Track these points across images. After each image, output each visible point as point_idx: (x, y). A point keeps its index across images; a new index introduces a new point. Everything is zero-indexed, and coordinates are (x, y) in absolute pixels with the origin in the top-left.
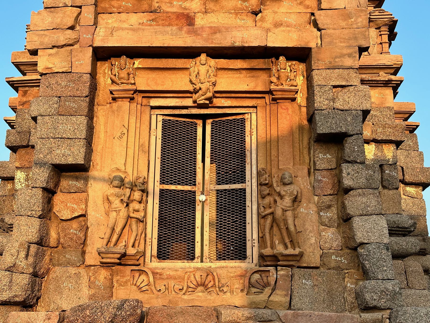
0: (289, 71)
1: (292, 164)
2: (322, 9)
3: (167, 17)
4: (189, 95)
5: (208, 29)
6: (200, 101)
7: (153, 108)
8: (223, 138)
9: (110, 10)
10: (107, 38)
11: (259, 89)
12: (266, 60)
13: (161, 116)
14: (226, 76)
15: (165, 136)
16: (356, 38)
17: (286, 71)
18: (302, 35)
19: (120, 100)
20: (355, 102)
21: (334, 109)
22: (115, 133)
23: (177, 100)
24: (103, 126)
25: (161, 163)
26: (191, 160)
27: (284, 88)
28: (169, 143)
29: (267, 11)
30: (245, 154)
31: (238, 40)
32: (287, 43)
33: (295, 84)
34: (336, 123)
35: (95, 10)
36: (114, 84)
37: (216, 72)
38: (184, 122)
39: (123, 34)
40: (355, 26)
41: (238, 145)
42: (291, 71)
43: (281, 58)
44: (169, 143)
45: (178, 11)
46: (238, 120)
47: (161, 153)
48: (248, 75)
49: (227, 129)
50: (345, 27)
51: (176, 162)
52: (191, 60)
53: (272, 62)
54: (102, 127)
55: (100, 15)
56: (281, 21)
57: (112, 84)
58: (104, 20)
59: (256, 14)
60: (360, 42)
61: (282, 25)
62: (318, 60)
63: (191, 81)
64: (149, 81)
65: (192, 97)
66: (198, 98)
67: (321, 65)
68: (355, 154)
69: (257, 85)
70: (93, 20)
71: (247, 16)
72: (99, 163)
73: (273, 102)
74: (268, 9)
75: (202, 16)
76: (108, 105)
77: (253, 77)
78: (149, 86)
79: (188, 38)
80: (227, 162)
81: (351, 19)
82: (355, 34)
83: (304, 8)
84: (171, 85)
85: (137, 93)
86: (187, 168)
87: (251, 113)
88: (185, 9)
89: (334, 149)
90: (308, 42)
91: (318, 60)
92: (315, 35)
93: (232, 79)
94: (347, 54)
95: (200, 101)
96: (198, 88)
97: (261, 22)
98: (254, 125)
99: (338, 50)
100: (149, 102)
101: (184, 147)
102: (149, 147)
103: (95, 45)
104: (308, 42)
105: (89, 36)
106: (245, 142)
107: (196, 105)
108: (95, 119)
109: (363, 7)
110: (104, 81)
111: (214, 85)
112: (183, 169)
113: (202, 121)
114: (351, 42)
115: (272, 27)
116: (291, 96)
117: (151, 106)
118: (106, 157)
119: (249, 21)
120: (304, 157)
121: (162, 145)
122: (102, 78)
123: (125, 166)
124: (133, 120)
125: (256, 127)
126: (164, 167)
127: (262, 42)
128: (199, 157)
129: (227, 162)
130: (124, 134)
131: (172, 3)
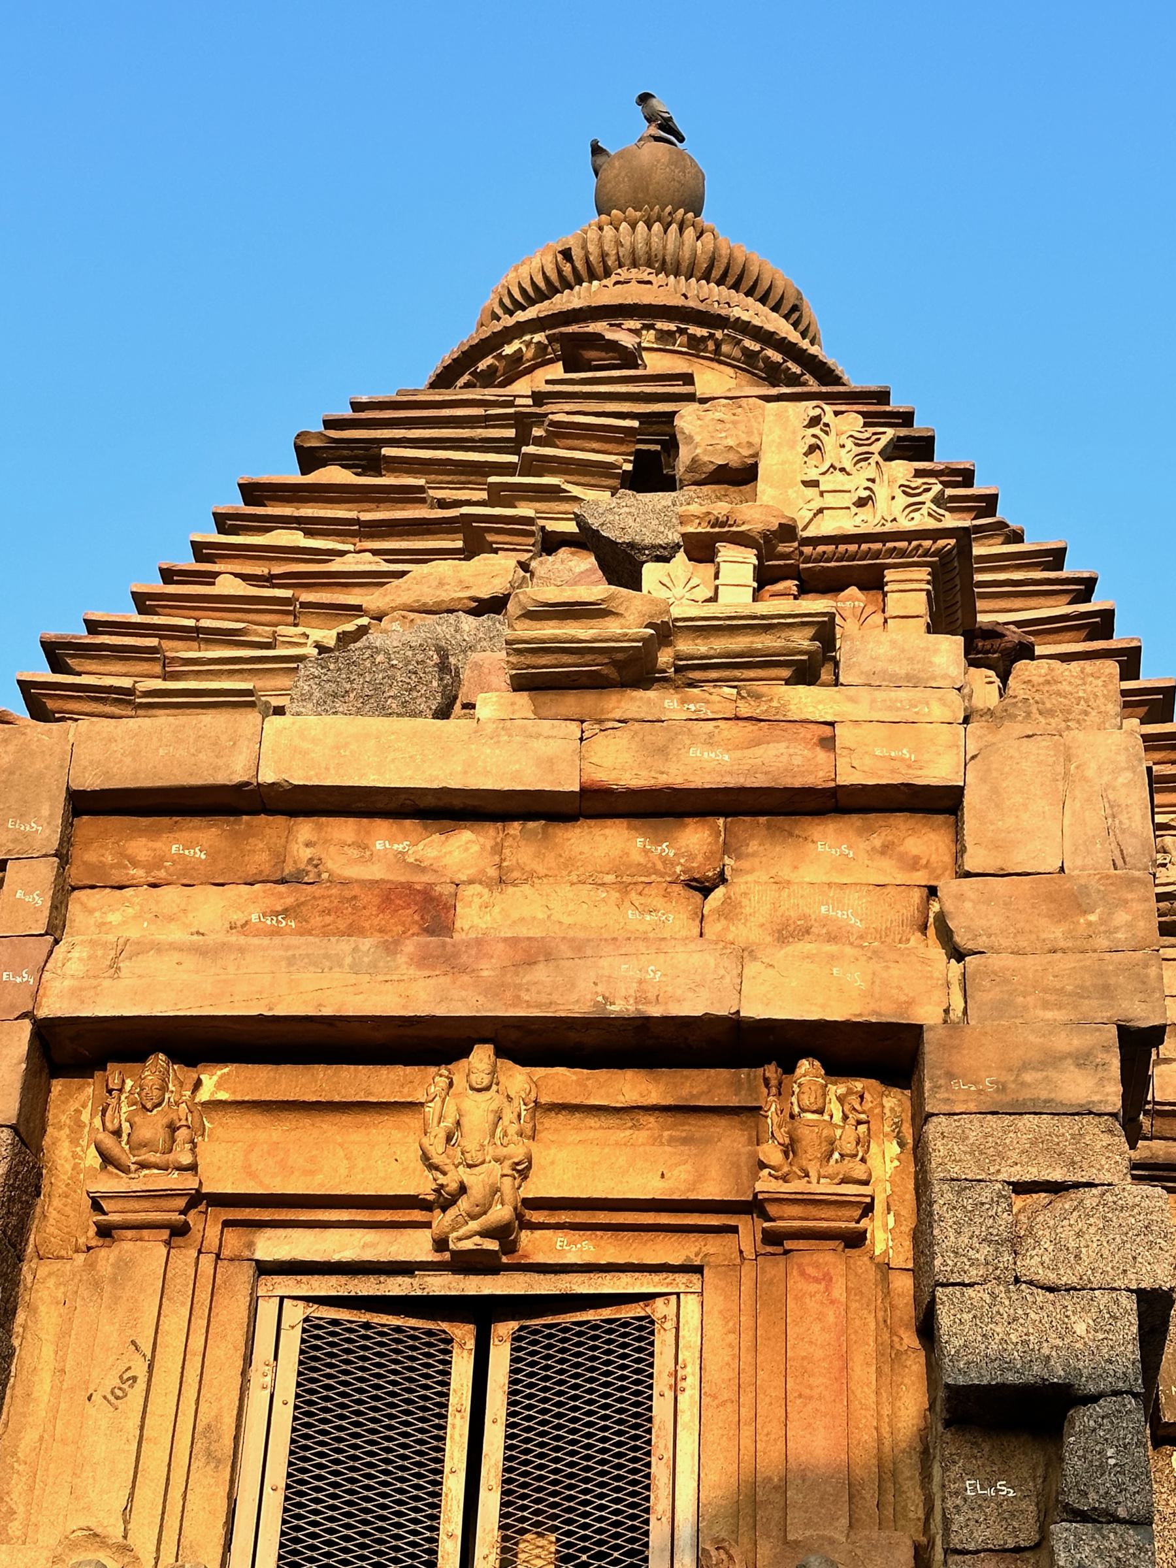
0: (838, 1118)
1: (845, 1521)
2: (968, 875)
3: (343, 900)
4: (417, 1215)
5: (501, 946)
6: (460, 1239)
7: (266, 1269)
8: (559, 1404)
9: (117, 877)
10: (94, 982)
11: (711, 1191)
12: (743, 1073)
13: (301, 1304)
14: (574, 1137)
15: (312, 1392)
16: (1106, 991)
17: (826, 1117)
18: (885, 975)
19: (129, 1234)
20: (1106, 1253)
21: (1017, 1280)
22: (95, 1373)
23: (370, 1236)
24: (52, 1348)
25: (286, 1510)
26: (417, 1498)
27: (815, 1188)
28: (325, 1421)
29: (750, 878)
30: (648, 1476)
31: (623, 993)
32: (823, 1007)
33: (859, 1172)
34: (1027, 1342)
35: (58, 875)
36: (110, 1168)
37: (533, 1118)
38: (398, 1329)
39: (161, 967)
40: (1103, 942)
41: (620, 1433)
42: (845, 1117)
43: (804, 1065)
44: (325, 1421)
45: (391, 878)
46: (626, 1324)
47: (290, 1464)
48: (666, 1134)
49: (577, 1365)
50: (1062, 944)
51: (353, 1510)
52: (433, 1070)
53: (767, 1082)
54: (48, 1352)
55: (76, 893)
56: (805, 917)
57: (103, 1168)
58: (91, 912)
59: (703, 887)
60: (1125, 1004)
61: (808, 932)
62: (950, 1076)
63: (425, 1158)
64: (254, 1156)
65: (427, 1225)
66: (454, 1229)
67: (962, 1097)
68: (1106, 1482)
69: (700, 1177)
70: (47, 913)
71: (666, 895)
72: (21, 1510)
73: (769, 1249)
74: (751, 871)
75: (485, 897)
76: (82, 1256)
77: (685, 1141)
78: (252, 1175)
79: (421, 983)
80: (570, 1510)
81: (1085, 912)
82: (1101, 974)
83: (900, 868)
84: (343, 1171)
85: (202, 1208)
86: (398, 1537)
87: (678, 1294)
88: (418, 867)
89: (1027, 1459)
90: (910, 1003)
91: (950, 1076)
92: (936, 974)
93: (597, 1150)
94: (1069, 1055)
95: (460, 1239)
96: (453, 1186)
97: (724, 922)
98: (688, 1347)
99: (1032, 1038)
100: (251, 1245)
101: (389, 1439)
102: (236, 1438)
103: (42, 1013)
104: (910, 1003)
105: (26, 978)
106: (650, 1420)
107: (447, 1256)
108: (21, 1316)
109: (1134, 867)
110: (75, 1156)
111: (523, 1171)
112: (381, 1542)
113: (472, 1326)
114: (1087, 1005)
115: (769, 939)
116: (843, 1225)
117: (257, 1261)
118: (50, 1481)
119: (674, 915)
120: (898, 1492)
121: (294, 1430)
122: (66, 1144)
123: (126, 1522)
124: (175, 1322)
125: (697, 1355)
126: (298, 1529)
127: (720, 1002)
128: (454, 1486)
129: (570, 1510)
130: (134, 1379)
131: (366, 847)
